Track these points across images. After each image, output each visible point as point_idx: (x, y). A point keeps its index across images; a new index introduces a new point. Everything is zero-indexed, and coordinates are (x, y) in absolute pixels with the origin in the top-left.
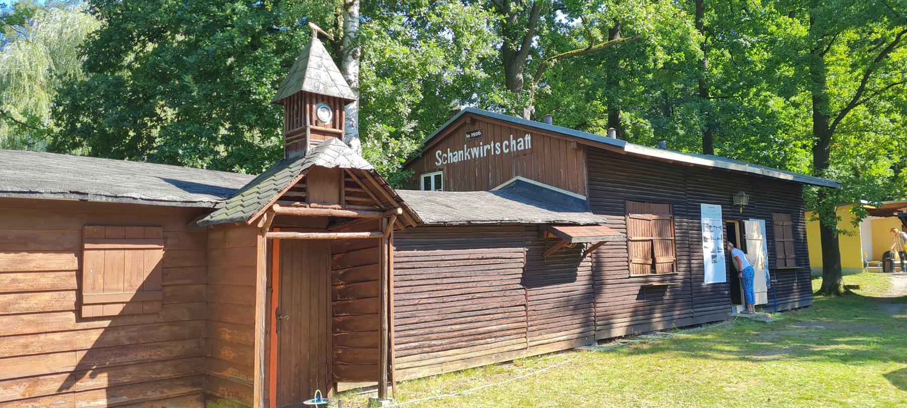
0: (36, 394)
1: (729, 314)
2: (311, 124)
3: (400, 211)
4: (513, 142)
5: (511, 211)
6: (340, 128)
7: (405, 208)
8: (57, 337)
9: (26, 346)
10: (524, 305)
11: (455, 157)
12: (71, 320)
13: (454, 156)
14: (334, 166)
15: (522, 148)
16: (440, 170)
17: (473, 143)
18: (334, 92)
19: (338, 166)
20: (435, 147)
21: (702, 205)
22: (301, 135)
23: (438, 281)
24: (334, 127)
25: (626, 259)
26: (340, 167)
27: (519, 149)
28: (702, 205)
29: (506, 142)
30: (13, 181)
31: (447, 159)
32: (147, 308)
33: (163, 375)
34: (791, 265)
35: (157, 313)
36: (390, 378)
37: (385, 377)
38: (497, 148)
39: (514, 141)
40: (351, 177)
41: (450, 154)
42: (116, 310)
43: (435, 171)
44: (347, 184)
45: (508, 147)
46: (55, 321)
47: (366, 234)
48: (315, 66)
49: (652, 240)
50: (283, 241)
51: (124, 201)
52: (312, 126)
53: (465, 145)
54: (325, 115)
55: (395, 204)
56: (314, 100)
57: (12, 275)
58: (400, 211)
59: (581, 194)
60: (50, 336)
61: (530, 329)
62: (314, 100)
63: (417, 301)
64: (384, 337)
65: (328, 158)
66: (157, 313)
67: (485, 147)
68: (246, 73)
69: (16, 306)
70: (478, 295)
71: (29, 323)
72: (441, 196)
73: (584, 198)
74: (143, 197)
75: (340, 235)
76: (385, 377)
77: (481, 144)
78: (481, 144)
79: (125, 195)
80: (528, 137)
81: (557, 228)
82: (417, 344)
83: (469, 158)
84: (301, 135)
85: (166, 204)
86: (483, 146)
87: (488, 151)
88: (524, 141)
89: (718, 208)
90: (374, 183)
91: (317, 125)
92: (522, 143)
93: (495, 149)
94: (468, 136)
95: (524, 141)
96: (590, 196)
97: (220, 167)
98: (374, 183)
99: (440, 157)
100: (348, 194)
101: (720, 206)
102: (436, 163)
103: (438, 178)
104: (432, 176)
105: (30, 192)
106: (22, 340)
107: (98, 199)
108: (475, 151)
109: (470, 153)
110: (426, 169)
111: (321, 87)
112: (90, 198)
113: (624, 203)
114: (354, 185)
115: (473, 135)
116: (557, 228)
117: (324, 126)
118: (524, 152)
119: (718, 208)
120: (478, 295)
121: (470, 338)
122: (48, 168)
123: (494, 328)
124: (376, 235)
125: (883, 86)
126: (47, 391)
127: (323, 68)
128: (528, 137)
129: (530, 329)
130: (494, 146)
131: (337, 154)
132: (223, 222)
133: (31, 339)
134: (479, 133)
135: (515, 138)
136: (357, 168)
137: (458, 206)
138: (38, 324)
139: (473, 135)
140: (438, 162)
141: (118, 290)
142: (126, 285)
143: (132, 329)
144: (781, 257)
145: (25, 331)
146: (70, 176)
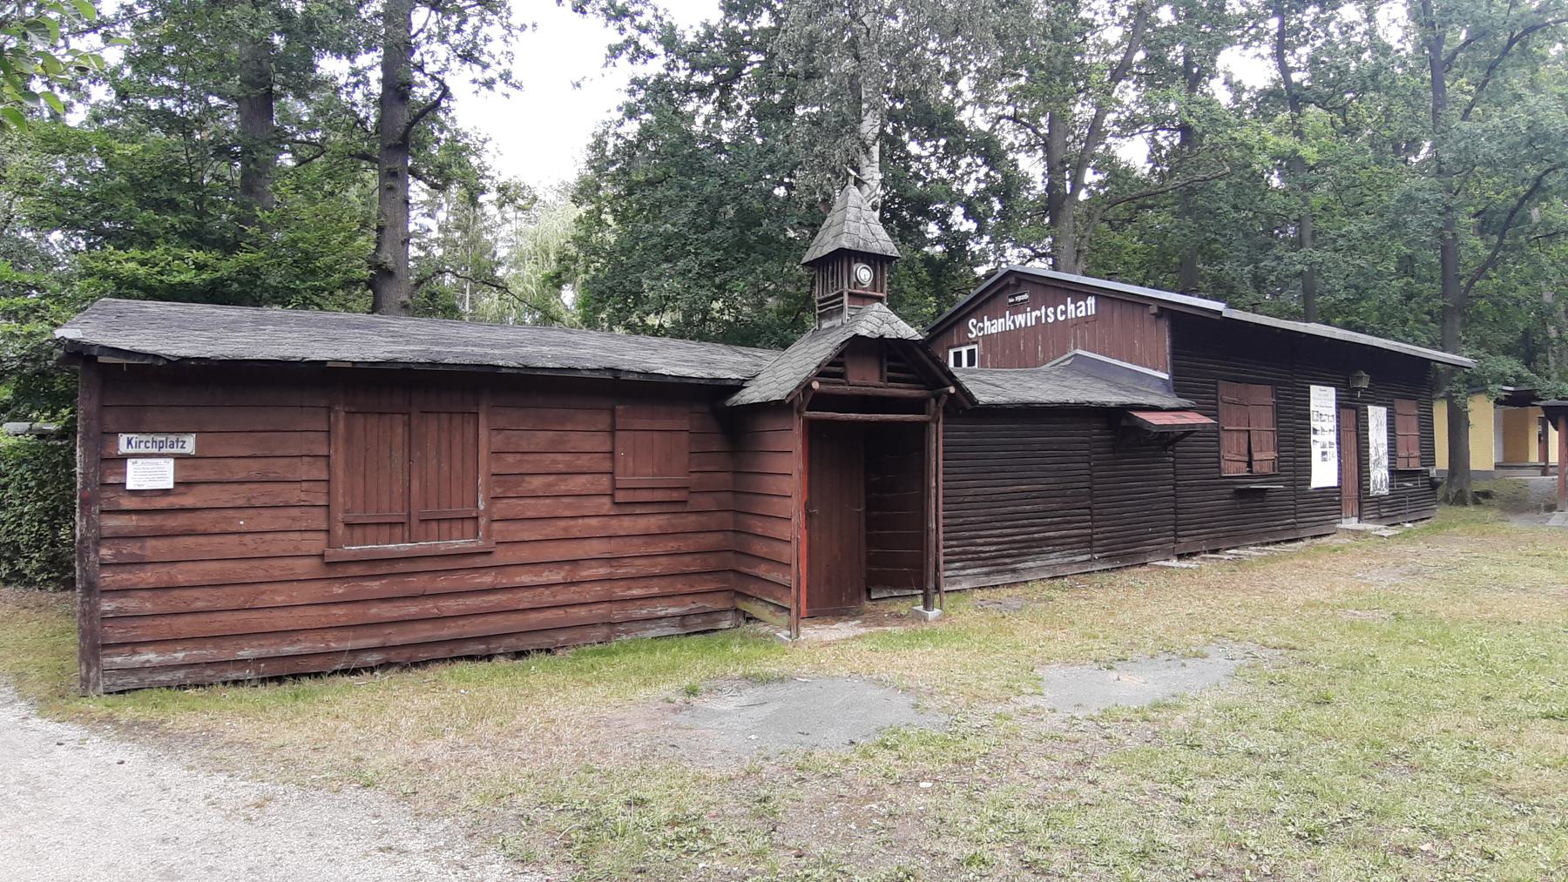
0: (577, 578)
1: (1338, 526)
3: (952, 390)
4: (1071, 307)
5: (1074, 392)
8: (594, 522)
9: (566, 529)
10: (1089, 508)
11: (994, 326)
13: (992, 325)
15: (1084, 314)
16: (974, 343)
17: (1017, 308)
18: (875, 248)
20: (968, 316)
21: (1312, 387)
22: (838, 300)
23: (986, 476)
25: (1179, 477)
26: (886, 337)
27: (1079, 315)
28: (1312, 387)
29: (1062, 307)
30: (554, 357)
31: (983, 329)
34: (1415, 465)
36: (937, 588)
37: (931, 585)
38: (1049, 314)
39: (1073, 306)
41: (987, 323)
43: (968, 344)
45: (1064, 313)
46: (591, 505)
48: (852, 218)
49: (1249, 431)
53: (1008, 313)
54: (864, 274)
55: (947, 381)
58: (952, 390)
59: (1162, 371)
60: (587, 521)
61: (1095, 536)
63: (961, 499)
67: (1034, 314)
69: (557, 488)
70: (1034, 494)
71: (567, 506)
72: (999, 377)
73: (1166, 377)
75: (861, 416)
76: (931, 585)
77: (1029, 309)
78: (1029, 309)
80: (1091, 301)
81: (1136, 414)
82: (960, 549)
83: (1012, 328)
84: (838, 300)
86: (1031, 312)
87: (1038, 319)
88: (1086, 305)
89: (1331, 391)
90: (923, 356)
92: (1083, 308)
93: (1047, 316)
94: (1011, 300)
95: (1086, 305)
96: (1175, 373)
97: (1438, 346)
98: (923, 356)
99: (975, 327)
101: (1333, 389)
102: (969, 335)
103: (971, 353)
104: (964, 351)
106: (563, 523)
107: (630, 377)
108: (1020, 319)
109: (1014, 322)
110: (955, 342)
111: (861, 242)
113: (1215, 383)
115: (1019, 298)
116: (1136, 414)
117: (863, 289)
118: (1086, 319)
119: (1331, 391)
120: (1034, 494)
121: (1023, 545)
122: (576, 345)
127: (862, 221)
128: (1091, 301)
129: (1095, 536)
130: (1046, 313)
132: (926, 434)
133: (572, 523)
134: (1026, 297)
135: (1074, 302)
137: (1007, 385)
139: (1019, 298)
140: (972, 333)
142: (655, 469)
144: (1404, 455)
145: (565, 514)
146: (599, 352)
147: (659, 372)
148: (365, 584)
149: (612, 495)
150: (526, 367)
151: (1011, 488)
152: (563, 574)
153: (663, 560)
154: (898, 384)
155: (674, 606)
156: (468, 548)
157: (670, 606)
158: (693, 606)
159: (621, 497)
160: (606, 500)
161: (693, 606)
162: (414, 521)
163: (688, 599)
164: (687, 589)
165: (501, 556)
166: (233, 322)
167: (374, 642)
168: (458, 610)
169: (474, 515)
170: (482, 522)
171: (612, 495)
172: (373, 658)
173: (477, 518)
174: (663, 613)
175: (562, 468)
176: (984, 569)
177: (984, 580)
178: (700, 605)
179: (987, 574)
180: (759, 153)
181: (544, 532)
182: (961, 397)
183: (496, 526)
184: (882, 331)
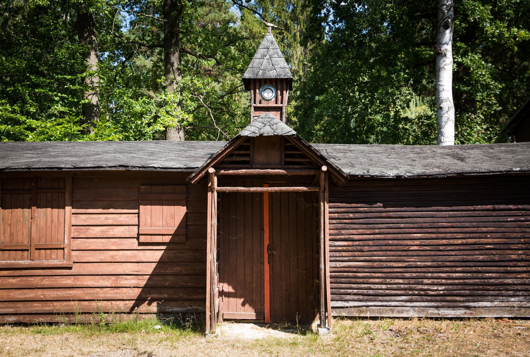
2: (255, 103)
6: (282, 103)
7: (329, 165)
12: (135, 243)
14: (258, 135)
19: (263, 134)
24: (276, 103)
32: (177, 239)
33: (189, 284)
35: (184, 243)
40: (290, 142)
42: (167, 239)
44: (286, 148)
47: (305, 189)
50: (271, 194)
51: (149, 169)
52: (255, 105)
56: (258, 84)
57: (106, 215)
62: (258, 84)
63: (406, 248)
64: (460, 276)
65: (253, 129)
66: (184, 243)
68: (98, 92)
74: (161, 166)
79: (149, 166)
85: (175, 170)
91: (260, 103)
100: (287, 156)
105: (99, 167)
111: (261, 72)
112: (129, 169)
114: (294, 148)
123: (510, 281)
124: (313, 189)
125: (189, 50)
126: (124, 284)
131: (264, 125)
136: (279, 134)
138: (120, 245)
141: (159, 226)
143: (170, 252)
147: (152, 166)
148: (9, 280)
149: (138, 238)
150: (75, 168)
151: (460, 241)
152: (110, 282)
153: (170, 278)
154: (293, 166)
155: (177, 307)
156: (58, 264)
157: (175, 307)
158: (190, 308)
159: (142, 239)
160: (135, 241)
161: (190, 308)
162: (33, 249)
163: (187, 303)
164: (185, 296)
165: (76, 269)
166: (152, 153)
167: (11, 310)
168: (54, 297)
169: (62, 247)
170: (66, 251)
171: (138, 238)
172: (12, 319)
173: (63, 249)
174: (170, 310)
175: (110, 222)
176: (433, 304)
177: (433, 312)
178: (195, 307)
179: (437, 307)
180: (49, 37)
181: (100, 258)
182: (331, 170)
183: (74, 253)
184: (262, 131)
